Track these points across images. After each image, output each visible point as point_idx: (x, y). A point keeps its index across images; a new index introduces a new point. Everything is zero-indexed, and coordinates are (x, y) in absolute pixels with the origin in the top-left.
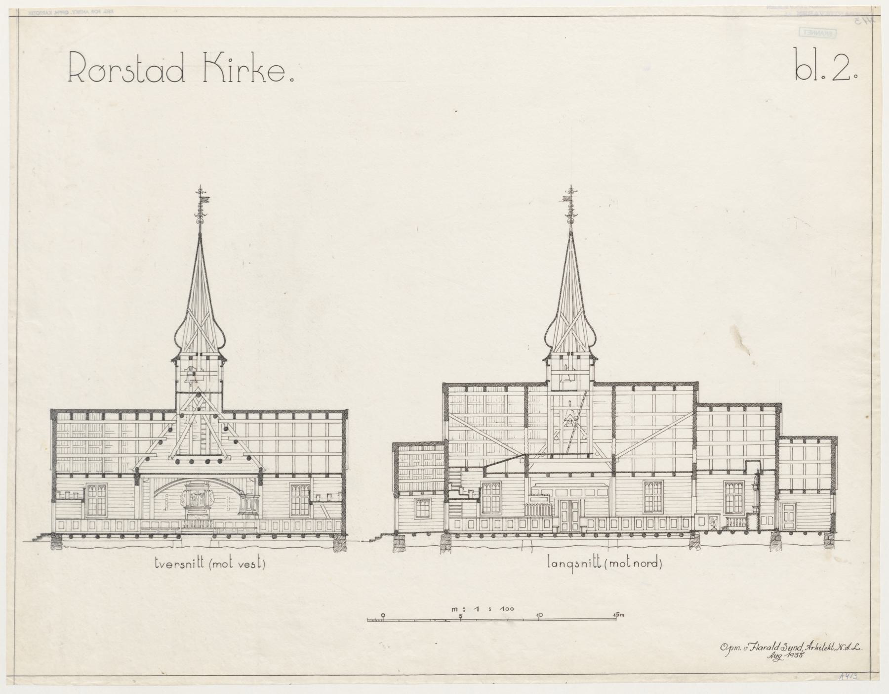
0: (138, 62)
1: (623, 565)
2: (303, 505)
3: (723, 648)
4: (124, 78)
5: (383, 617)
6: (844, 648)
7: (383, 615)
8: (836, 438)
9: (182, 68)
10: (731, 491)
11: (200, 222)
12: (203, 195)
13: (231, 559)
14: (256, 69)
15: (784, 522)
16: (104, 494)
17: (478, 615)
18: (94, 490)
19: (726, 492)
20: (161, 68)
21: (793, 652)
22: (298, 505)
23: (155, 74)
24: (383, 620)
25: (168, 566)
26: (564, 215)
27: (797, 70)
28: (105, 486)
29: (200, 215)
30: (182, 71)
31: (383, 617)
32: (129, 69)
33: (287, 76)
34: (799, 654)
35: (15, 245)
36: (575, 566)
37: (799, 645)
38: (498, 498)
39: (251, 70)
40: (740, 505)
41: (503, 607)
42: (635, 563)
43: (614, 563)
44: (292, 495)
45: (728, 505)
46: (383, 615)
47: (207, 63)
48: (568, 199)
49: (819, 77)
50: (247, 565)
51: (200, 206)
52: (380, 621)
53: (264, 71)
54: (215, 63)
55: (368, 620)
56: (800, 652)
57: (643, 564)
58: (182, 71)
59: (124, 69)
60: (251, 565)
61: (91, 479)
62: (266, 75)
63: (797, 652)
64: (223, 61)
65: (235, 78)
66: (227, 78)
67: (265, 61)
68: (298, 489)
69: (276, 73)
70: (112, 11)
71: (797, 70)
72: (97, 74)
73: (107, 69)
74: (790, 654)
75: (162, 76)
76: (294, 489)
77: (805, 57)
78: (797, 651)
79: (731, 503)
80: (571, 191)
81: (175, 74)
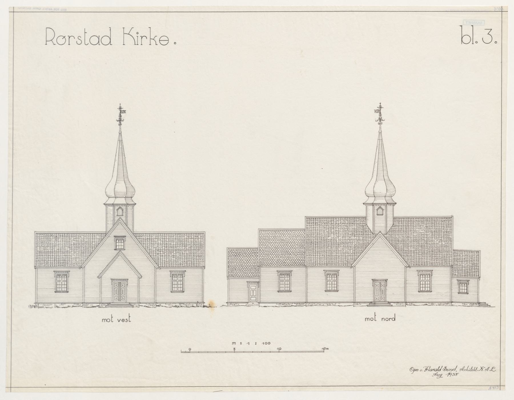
0: (85, 33)
1: (372, 319)
5: (190, 350)
7: (190, 349)
9: (110, 37)
10: (283, 279)
12: (122, 110)
13: (129, 317)
15: (250, 297)
16: (181, 279)
17: (256, 348)
18: (60, 277)
19: (420, 279)
20: (98, 37)
23: (95, 40)
24: (189, 352)
25: (123, 321)
26: (116, 120)
27: (462, 38)
28: (67, 275)
29: (120, 120)
30: (110, 39)
31: (190, 350)
32: (79, 38)
33: (171, 42)
39: (148, 38)
42: (382, 319)
43: (367, 319)
44: (173, 280)
45: (181, 285)
46: (190, 349)
48: (379, 111)
49: (474, 42)
50: (123, 320)
51: (120, 116)
52: (188, 352)
53: (157, 39)
54: (129, 34)
55: (182, 352)
57: (387, 319)
58: (110, 39)
59: (76, 37)
60: (125, 320)
61: (322, 269)
62: (158, 43)
64: (133, 33)
65: (140, 43)
68: (330, 276)
69: (164, 41)
71: (462, 38)
72: (61, 41)
73: (67, 38)
75: (99, 42)
76: (58, 277)
77: (467, 30)
79: (176, 285)
80: (381, 107)
81: (106, 40)
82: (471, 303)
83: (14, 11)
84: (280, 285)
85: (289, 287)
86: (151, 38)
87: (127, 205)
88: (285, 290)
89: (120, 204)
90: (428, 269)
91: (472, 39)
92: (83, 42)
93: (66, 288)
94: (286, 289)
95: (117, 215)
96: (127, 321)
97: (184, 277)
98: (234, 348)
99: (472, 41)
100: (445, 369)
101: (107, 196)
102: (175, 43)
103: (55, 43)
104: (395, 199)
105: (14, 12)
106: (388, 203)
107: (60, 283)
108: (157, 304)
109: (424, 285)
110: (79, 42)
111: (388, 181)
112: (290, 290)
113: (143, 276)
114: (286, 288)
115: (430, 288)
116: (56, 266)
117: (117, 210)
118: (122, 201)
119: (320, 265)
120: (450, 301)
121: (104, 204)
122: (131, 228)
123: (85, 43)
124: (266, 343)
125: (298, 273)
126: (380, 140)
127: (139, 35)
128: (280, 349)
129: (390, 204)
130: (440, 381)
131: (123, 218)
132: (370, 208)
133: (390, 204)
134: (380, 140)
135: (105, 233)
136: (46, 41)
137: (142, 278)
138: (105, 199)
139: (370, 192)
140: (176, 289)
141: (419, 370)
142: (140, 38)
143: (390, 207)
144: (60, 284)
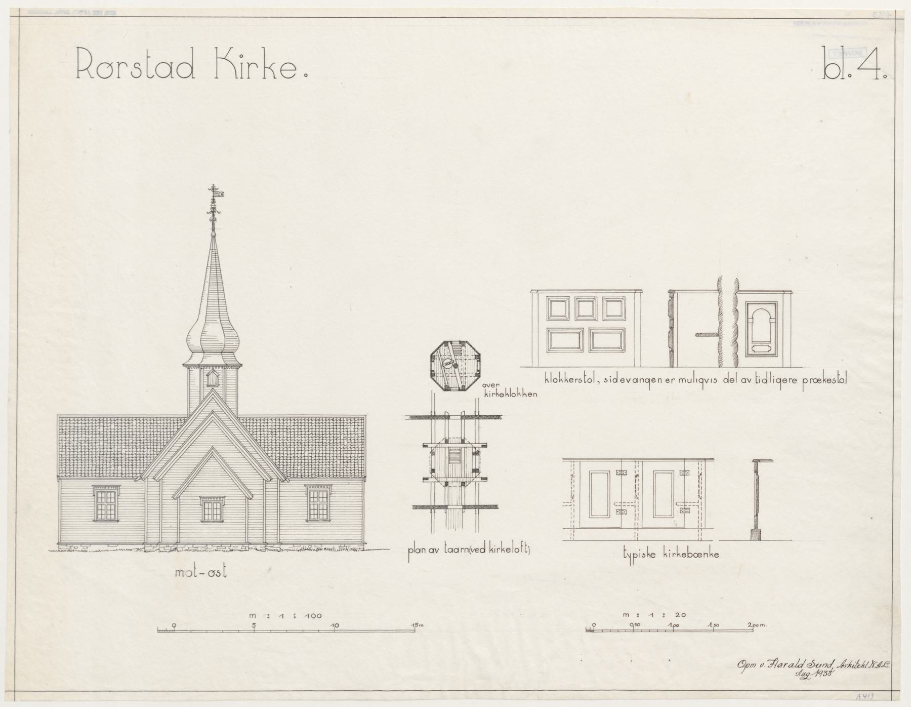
0: (148, 57)
2: (215, 510)
3: (741, 665)
4: (133, 73)
6: (876, 665)
7: (174, 625)
8: (486, 447)
9: (191, 65)
11: (213, 220)
14: (268, 65)
20: (170, 64)
21: (821, 669)
22: (210, 510)
23: (164, 70)
24: (174, 631)
27: (825, 69)
30: (192, 69)
32: (137, 65)
33: (300, 73)
34: (828, 672)
35: (16, 240)
36: (216, 575)
37: (829, 663)
38: (325, 506)
40: (219, 513)
41: (671, 624)
44: (310, 501)
47: (218, 59)
49: (846, 76)
51: (213, 201)
53: (276, 69)
55: (159, 631)
56: (830, 669)
58: (192, 69)
59: (131, 65)
63: (826, 670)
64: (234, 56)
65: (245, 75)
66: (239, 75)
67: (277, 58)
69: (288, 70)
70: (47, 13)
71: (825, 69)
72: (105, 71)
73: (115, 66)
74: (818, 672)
78: (826, 669)
81: (185, 70)
82: (193, 544)
83: (18, 18)
84: (310, 512)
85: (327, 514)
86: (79, 69)
87: (225, 366)
88: (106, 519)
89: (213, 365)
90: (111, 483)
91: (841, 70)
92: (144, 73)
93: (310, 514)
94: (215, 518)
95: (208, 386)
96: (218, 574)
97: (119, 497)
98: (254, 624)
99: (841, 75)
100: (813, 663)
101: (190, 349)
102: (306, 75)
103: (94, 73)
104: (240, 357)
105: (19, 16)
106: (227, 365)
107: (316, 506)
108: (278, 545)
109: (316, 511)
110: (136, 73)
111: (227, 326)
112: (116, 519)
113: (255, 496)
114: (215, 516)
115: (221, 517)
116: (296, 476)
117: (207, 375)
118: (217, 359)
119: (85, 476)
120: (361, 541)
121: (183, 365)
122: (234, 410)
123: (148, 74)
124: (313, 616)
125: (130, 491)
126: (214, 253)
127: (244, 60)
128: (336, 625)
129: (232, 366)
130: (805, 685)
131: (219, 390)
132: (196, 372)
133: (232, 366)
134: (214, 253)
135: (187, 416)
136: (78, 71)
137: (253, 498)
138: (185, 355)
139: (196, 342)
140: (103, 517)
141: (758, 665)
142: (245, 66)
143: (231, 372)
144: (103, 508)
